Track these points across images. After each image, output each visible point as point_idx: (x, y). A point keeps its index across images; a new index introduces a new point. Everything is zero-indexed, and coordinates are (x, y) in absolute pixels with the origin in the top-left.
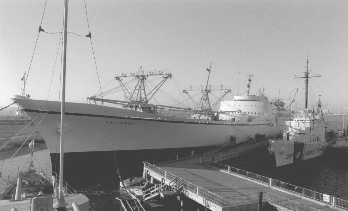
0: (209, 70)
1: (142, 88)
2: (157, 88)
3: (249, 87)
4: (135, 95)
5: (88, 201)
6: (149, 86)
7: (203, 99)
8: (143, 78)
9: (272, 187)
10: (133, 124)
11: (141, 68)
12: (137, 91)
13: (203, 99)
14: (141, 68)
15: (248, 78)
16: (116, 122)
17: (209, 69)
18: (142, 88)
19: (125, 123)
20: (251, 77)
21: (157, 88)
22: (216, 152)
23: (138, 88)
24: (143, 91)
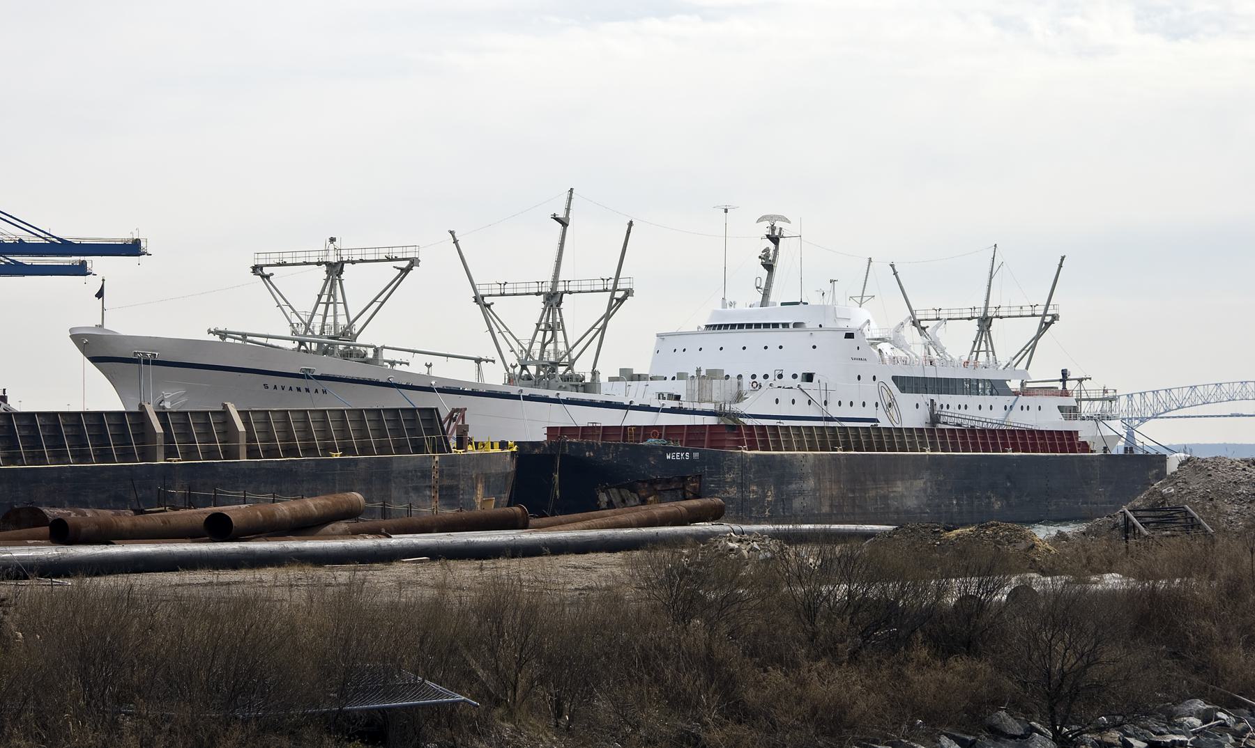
0: (564, 223)
1: (340, 299)
2: (380, 300)
3: (769, 267)
4: (318, 320)
5: (506, 476)
6: (360, 284)
7: (543, 327)
8: (335, 269)
9: (1186, 739)
10: (324, 392)
11: (332, 240)
12: (322, 308)
13: (543, 327)
14: (332, 240)
15: (764, 229)
16: (287, 388)
17: (561, 215)
18: (340, 299)
19: (307, 390)
20: (778, 224)
21: (380, 300)
22: (607, 520)
23: (324, 299)
24: (340, 308)
